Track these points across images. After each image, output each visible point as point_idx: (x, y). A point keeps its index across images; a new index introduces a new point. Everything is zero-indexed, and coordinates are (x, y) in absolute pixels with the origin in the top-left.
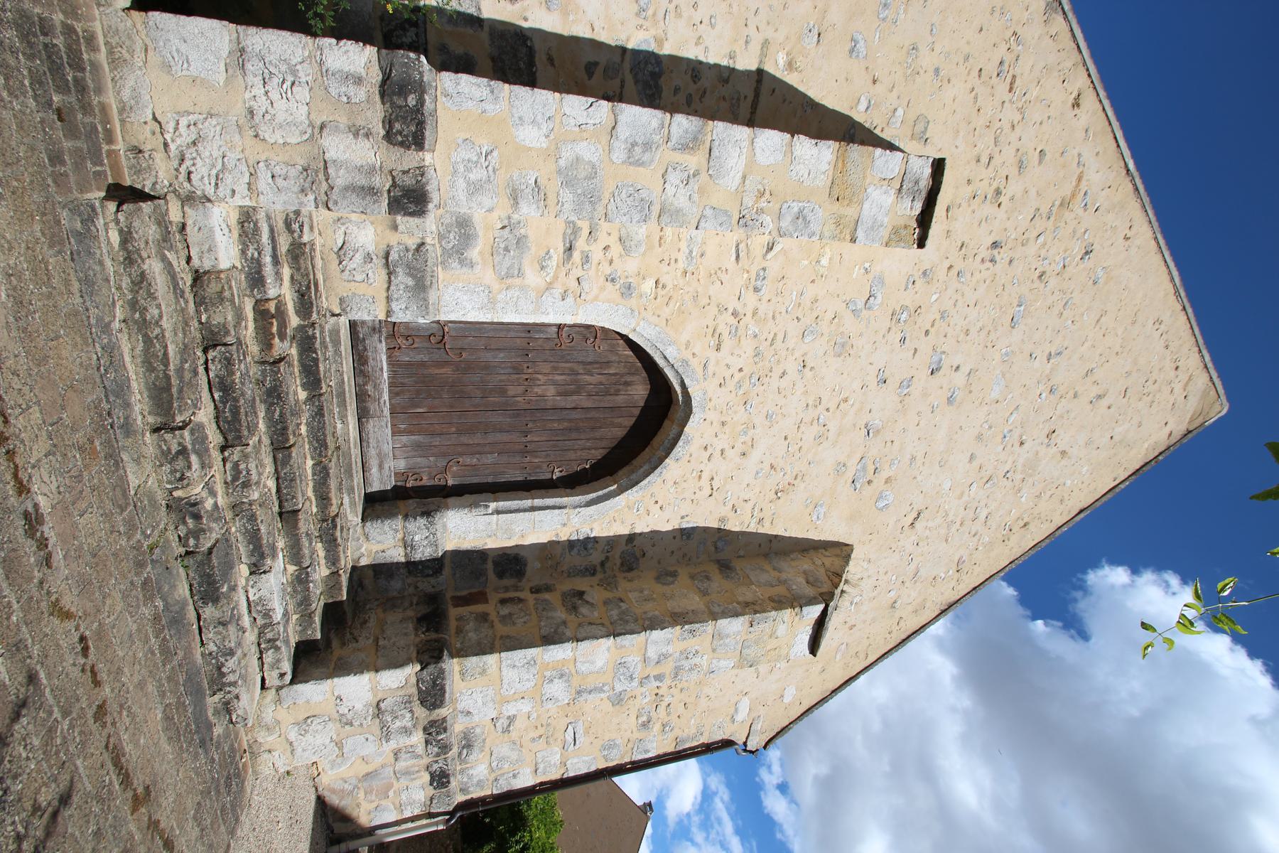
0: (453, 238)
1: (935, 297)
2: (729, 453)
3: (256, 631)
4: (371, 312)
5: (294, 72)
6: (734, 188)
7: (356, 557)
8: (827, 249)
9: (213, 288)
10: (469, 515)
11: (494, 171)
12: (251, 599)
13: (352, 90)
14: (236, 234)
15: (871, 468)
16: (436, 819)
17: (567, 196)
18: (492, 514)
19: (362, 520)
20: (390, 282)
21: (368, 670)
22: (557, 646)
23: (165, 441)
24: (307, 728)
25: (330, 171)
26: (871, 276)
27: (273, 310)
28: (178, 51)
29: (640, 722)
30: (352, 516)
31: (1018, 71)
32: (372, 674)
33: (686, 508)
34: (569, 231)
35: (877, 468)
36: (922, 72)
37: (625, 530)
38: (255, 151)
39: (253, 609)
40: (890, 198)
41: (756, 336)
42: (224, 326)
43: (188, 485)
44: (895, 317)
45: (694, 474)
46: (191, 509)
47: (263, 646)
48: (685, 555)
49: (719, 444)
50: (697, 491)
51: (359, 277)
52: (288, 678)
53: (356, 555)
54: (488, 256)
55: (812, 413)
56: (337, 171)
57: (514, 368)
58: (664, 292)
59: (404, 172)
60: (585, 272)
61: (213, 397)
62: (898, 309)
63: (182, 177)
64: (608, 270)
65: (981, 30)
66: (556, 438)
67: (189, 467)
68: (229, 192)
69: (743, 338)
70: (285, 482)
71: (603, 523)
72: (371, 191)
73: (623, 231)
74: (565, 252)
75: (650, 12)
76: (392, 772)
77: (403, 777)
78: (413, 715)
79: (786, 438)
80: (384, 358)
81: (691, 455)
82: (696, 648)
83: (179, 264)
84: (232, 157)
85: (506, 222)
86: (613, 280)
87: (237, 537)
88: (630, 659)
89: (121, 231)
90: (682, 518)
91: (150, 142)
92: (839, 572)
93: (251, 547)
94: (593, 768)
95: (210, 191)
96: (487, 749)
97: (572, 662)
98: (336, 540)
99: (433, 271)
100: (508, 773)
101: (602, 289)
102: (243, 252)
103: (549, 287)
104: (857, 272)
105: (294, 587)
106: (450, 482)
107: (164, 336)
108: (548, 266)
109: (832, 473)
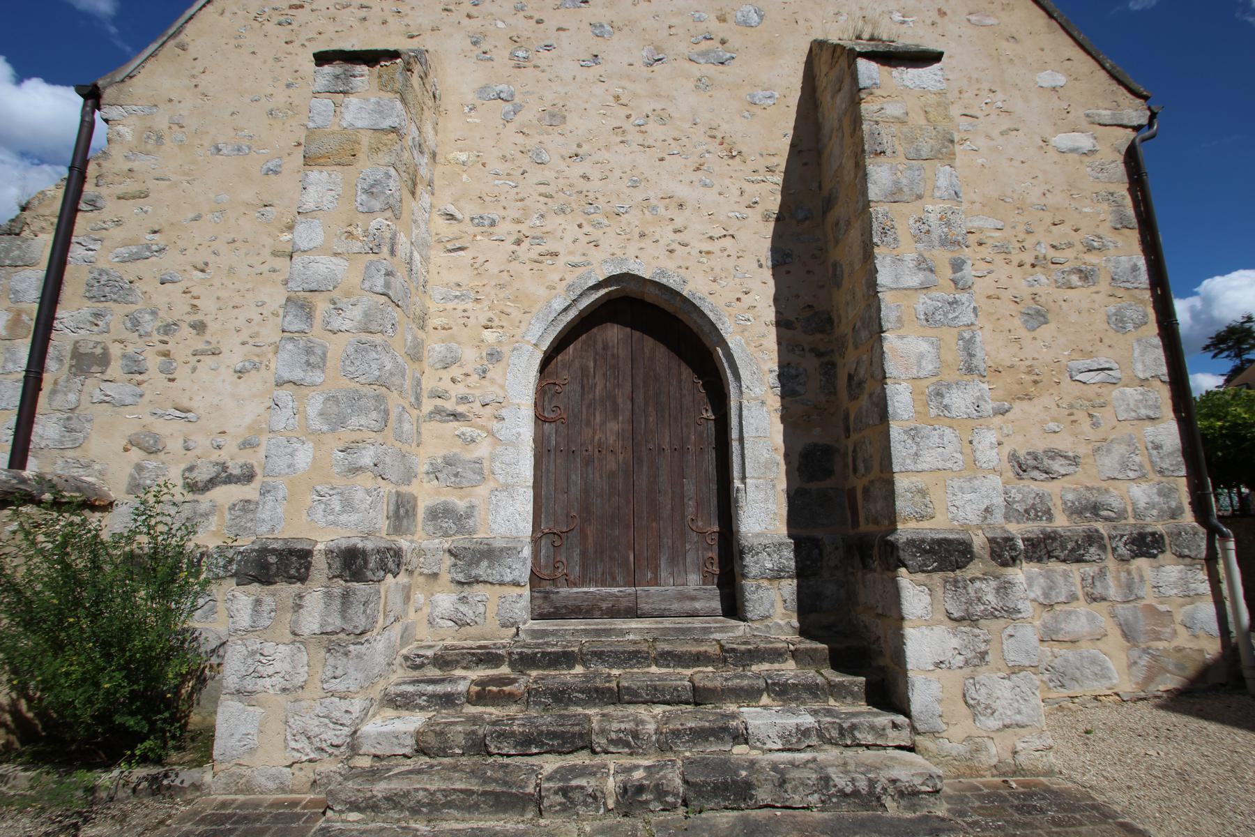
0: (448, 524)
1: (500, 24)
2: (679, 223)
3: (826, 747)
4: (520, 601)
5: (253, 653)
6: (346, 263)
7: (791, 631)
8: (451, 156)
9: (432, 740)
10: (745, 509)
11: (333, 489)
12: (780, 747)
13: (266, 608)
14: (405, 713)
15: (705, 45)
16: (1219, 550)
17: (354, 421)
18: (745, 484)
19: (744, 621)
20: (485, 582)
21: (901, 628)
22: (889, 403)
23: (551, 806)
24: (983, 706)
25: (329, 630)
26: (478, 103)
27: (478, 688)
28: (240, 741)
29: (1080, 284)
30: (740, 629)
31: (285, 5)
32: (906, 624)
33: (749, 264)
34: (438, 417)
35: (705, 38)
36: (290, 100)
37: (773, 332)
38: (315, 690)
39: (796, 747)
40: (353, 101)
41: (542, 216)
42: (466, 734)
43: (602, 792)
44: (522, 64)
45: (704, 260)
46: (629, 794)
47: (849, 742)
48: (814, 257)
49: (666, 235)
50: (726, 253)
51: (482, 609)
52: (900, 719)
53: (788, 629)
54: (462, 492)
55: (634, 137)
56: (329, 624)
57: (587, 465)
58: (496, 319)
59: (330, 568)
60: (477, 400)
61: (536, 754)
62: (513, 63)
63: (336, 752)
64: (475, 377)
65: (253, 53)
66: (667, 416)
67: (582, 788)
68: (347, 715)
69: (544, 230)
70: (655, 696)
71: (763, 359)
72: (346, 596)
73: (438, 366)
74: (458, 420)
75: (256, 359)
76: (1125, 606)
77: (1136, 591)
78: (978, 579)
79: (662, 160)
80: (575, 590)
81: (680, 267)
82: (911, 222)
83: (410, 764)
84: (319, 710)
85: (432, 476)
86: (484, 372)
87: (698, 753)
88: (921, 308)
89: (350, 810)
90: (761, 266)
91: (304, 775)
92: (832, 50)
93: (712, 739)
94: (1157, 341)
95: (346, 731)
96: (1105, 485)
97: (918, 382)
98: (749, 651)
99: (477, 542)
100: (1150, 456)
101: (493, 381)
102: (422, 708)
103: (491, 433)
104: (474, 119)
105: (791, 700)
106: (716, 528)
107: (444, 790)
108: (471, 436)
109: (710, 93)
